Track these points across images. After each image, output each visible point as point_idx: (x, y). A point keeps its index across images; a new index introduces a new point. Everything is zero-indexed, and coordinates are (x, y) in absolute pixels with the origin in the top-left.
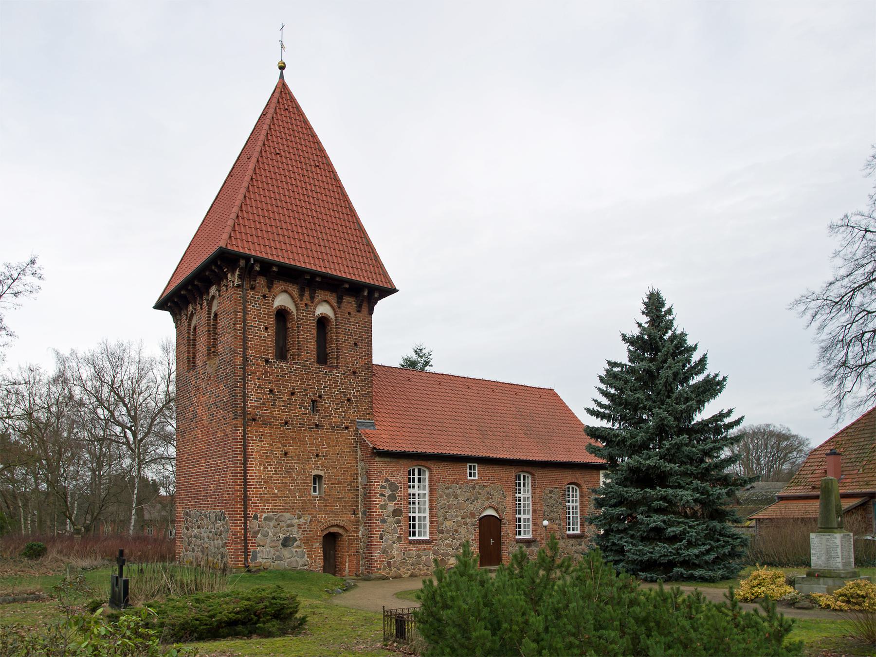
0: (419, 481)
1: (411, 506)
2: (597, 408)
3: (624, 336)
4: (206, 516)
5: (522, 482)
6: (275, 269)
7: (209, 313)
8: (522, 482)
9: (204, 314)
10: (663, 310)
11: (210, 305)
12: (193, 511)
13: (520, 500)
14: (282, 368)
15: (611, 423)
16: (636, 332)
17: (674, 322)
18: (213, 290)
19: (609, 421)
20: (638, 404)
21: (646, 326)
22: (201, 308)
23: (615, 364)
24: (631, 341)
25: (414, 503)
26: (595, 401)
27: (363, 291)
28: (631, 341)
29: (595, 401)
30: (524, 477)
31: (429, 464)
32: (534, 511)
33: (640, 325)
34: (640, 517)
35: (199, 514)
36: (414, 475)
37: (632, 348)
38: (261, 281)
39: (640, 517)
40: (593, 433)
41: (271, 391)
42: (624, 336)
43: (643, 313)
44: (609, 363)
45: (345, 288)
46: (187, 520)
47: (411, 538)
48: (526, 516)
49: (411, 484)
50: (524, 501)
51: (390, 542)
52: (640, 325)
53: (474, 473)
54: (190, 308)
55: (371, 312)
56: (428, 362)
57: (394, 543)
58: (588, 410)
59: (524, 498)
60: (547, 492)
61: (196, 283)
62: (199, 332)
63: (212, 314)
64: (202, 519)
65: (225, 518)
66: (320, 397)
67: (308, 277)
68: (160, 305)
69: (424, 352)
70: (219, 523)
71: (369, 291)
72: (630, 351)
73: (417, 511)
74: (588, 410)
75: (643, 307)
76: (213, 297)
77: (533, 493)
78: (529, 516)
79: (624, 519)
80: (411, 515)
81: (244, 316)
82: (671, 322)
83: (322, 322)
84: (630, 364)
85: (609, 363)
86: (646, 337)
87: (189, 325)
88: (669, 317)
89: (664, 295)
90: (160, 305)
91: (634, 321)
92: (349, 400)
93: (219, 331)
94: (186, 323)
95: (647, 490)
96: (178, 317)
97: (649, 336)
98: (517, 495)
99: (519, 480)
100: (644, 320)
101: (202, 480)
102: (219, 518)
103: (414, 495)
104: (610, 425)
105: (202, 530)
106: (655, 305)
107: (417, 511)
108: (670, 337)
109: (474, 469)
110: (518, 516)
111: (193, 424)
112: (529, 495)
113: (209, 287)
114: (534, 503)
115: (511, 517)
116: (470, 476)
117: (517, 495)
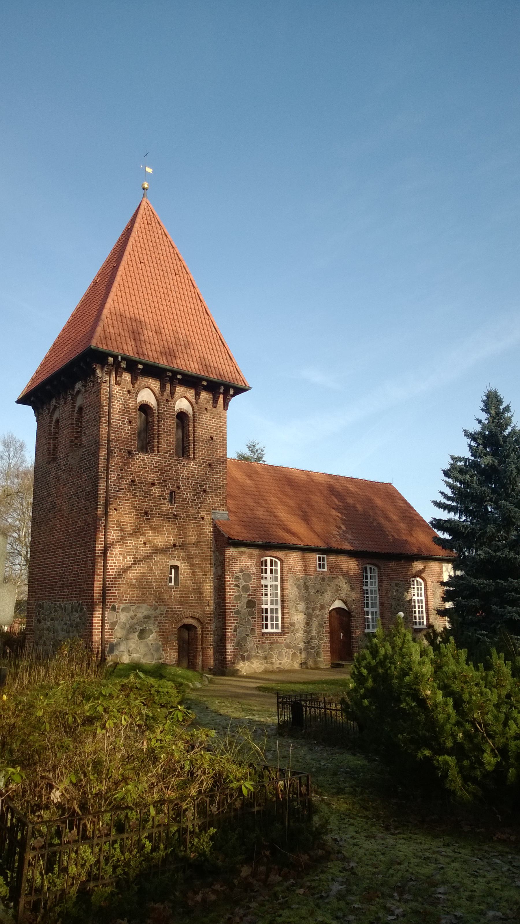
0: (271, 572)
1: (264, 598)
2: (444, 501)
3: (465, 432)
4: (60, 607)
5: (369, 574)
6: (140, 366)
7: (73, 407)
8: (369, 574)
9: (68, 408)
10: (501, 407)
11: (74, 399)
12: (47, 604)
13: (367, 593)
14: (143, 460)
15: (458, 515)
16: (478, 428)
17: (513, 419)
18: (79, 385)
19: (455, 513)
20: (486, 496)
21: (486, 422)
22: (65, 403)
23: (460, 459)
24: (473, 437)
25: (266, 595)
26: (442, 493)
27: (220, 389)
28: (473, 437)
29: (442, 493)
30: (371, 569)
31: (280, 554)
32: (382, 604)
33: (480, 422)
34: (494, 607)
35: (53, 605)
36: (266, 565)
37: (473, 444)
38: (127, 377)
39: (494, 607)
40: (439, 524)
41: (133, 481)
42: (465, 432)
43: (483, 410)
44: (453, 458)
45: (203, 385)
46: (39, 612)
47: (264, 630)
48: (374, 610)
49: (264, 575)
50: (372, 593)
51: (244, 635)
52: (480, 422)
53: (324, 565)
54: (53, 402)
55: (226, 405)
56: (261, 458)
57: (248, 635)
58: (435, 503)
59: (371, 591)
60: (393, 585)
61: (62, 379)
62: (61, 424)
63: (77, 408)
64: (56, 611)
65: (82, 609)
66: (178, 487)
67: (170, 374)
68: (23, 400)
69: (257, 447)
70: (76, 615)
71: (223, 389)
72: (470, 446)
73: (269, 603)
74: (435, 503)
75: (482, 405)
76: (79, 392)
77: (380, 586)
78: (376, 609)
79: (477, 611)
80: (264, 607)
81: (109, 410)
82: (510, 418)
83: (182, 416)
84: (473, 458)
85: (453, 458)
86: (487, 433)
87: (51, 418)
88: (507, 415)
89: (501, 394)
90: (23, 400)
91: (474, 418)
92: (205, 491)
93: (84, 424)
94: (48, 417)
95: (499, 581)
96: (41, 411)
97: (490, 432)
98: (365, 588)
99: (366, 572)
100: (484, 417)
101: (58, 571)
102: (74, 609)
103: (266, 586)
104: (457, 518)
105: (56, 623)
106: (492, 402)
107: (269, 603)
108: (510, 433)
109: (323, 561)
110: (366, 609)
111: (51, 515)
112: (376, 587)
113: (75, 383)
114: (381, 596)
115: (360, 610)
116: (320, 568)
117: (365, 588)
